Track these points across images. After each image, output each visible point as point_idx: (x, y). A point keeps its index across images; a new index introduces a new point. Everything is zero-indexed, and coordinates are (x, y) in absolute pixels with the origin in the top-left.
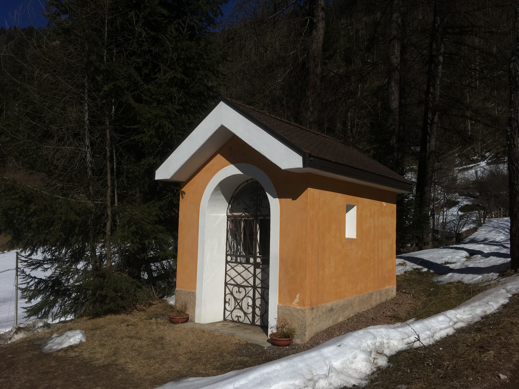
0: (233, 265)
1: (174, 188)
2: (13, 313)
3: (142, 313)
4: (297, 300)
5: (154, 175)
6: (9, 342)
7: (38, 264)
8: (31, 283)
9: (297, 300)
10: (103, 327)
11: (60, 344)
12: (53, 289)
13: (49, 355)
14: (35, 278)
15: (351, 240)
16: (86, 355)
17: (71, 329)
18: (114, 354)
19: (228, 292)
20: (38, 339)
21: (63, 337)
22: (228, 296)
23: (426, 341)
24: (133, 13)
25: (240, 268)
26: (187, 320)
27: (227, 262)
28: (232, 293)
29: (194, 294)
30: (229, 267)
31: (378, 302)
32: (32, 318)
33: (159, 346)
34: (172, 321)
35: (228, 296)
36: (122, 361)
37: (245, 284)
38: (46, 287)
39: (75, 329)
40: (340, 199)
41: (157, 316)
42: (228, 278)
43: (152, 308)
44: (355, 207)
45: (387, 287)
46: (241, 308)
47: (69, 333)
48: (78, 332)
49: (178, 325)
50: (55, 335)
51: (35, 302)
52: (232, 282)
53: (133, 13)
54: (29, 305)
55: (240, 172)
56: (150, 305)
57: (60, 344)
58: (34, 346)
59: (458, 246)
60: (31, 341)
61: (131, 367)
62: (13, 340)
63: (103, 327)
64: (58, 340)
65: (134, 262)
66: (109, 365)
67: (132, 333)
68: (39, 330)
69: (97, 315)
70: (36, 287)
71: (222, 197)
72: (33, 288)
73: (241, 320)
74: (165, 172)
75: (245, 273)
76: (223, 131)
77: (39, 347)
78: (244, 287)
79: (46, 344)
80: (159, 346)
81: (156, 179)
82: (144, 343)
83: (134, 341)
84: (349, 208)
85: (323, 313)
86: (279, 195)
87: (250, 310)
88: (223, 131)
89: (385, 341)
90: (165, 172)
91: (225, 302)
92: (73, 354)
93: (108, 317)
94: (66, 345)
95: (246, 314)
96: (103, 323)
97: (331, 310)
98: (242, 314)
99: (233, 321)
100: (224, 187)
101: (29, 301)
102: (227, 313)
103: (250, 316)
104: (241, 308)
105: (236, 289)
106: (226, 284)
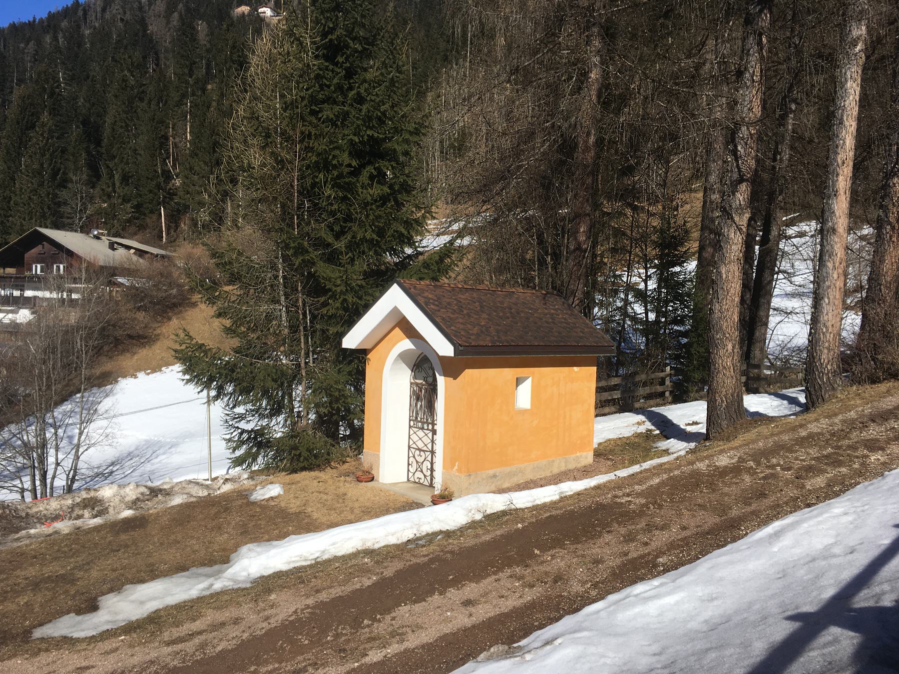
0: (415, 430)
1: (360, 355)
2: (206, 451)
3: (335, 471)
4: (456, 467)
5: (340, 343)
6: (219, 492)
7: (241, 417)
8: (234, 434)
9: (456, 467)
10: (299, 482)
11: (263, 495)
12: (258, 441)
13: (254, 503)
14: (238, 428)
15: (524, 412)
16: (283, 504)
17: (271, 483)
18: (305, 505)
19: (411, 455)
20: (245, 490)
21: (265, 489)
22: (411, 459)
23: (520, 505)
24: (321, 176)
25: (421, 433)
26: (373, 479)
27: (410, 427)
28: (414, 457)
29: (378, 456)
30: (412, 432)
31: (563, 469)
32: (238, 469)
33: (341, 501)
34: (359, 480)
35: (411, 459)
36: (310, 510)
37: (425, 448)
38: (249, 438)
39: (276, 483)
40: (508, 374)
41: (347, 475)
42: (411, 442)
43: (346, 466)
44: (530, 379)
45: (578, 454)
46: (422, 471)
47: (270, 486)
48: (277, 485)
49: (363, 483)
50: (258, 487)
51: (238, 453)
52: (414, 446)
53: (321, 176)
54: (233, 456)
55: (413, 347)
56: (344, 462)
57: (263, 495)
58: (242, 495)
59: (17, 536)
60: (239, 491)
61: (315, 515)
62: (222, 491)
63: (299, 482)
64: (261, 492)
65: (327, 424)
66: (300, 513)
67: (321, 489)
68: (245, 482)
69: (294, 471)
70: (240, 437)
71: (404, 365)
72: (236, 439)
73: (421, 481)
74: (351, 341)
75: (422, 438)
76: (396, 310)
77: (247, 497)
78: (424, 451)
79: (251, 494)
80: (341, 501)
81: (344, 346)
82: (329, 498)
83: (322, 495)
84: (519, 381)
85: (483, 479)
86: (446, 374)
87: (429, 472)
88: (396, 310)
89: (490, 503)
90: (351, 341)
91: (409, 464)
92: (273, 504)
93: (304, 473)
94: (267, 496)
95: (425, 476)
96: (298, 479)
97: (495, 476)
98: (423, 477)
99: (415, 482)
100: (403, 357)
101: (234, 450)
102: (411, 475)
103: (429, 478)
104: (422, 471)
105: (417, 452)
106: (409, 447)
